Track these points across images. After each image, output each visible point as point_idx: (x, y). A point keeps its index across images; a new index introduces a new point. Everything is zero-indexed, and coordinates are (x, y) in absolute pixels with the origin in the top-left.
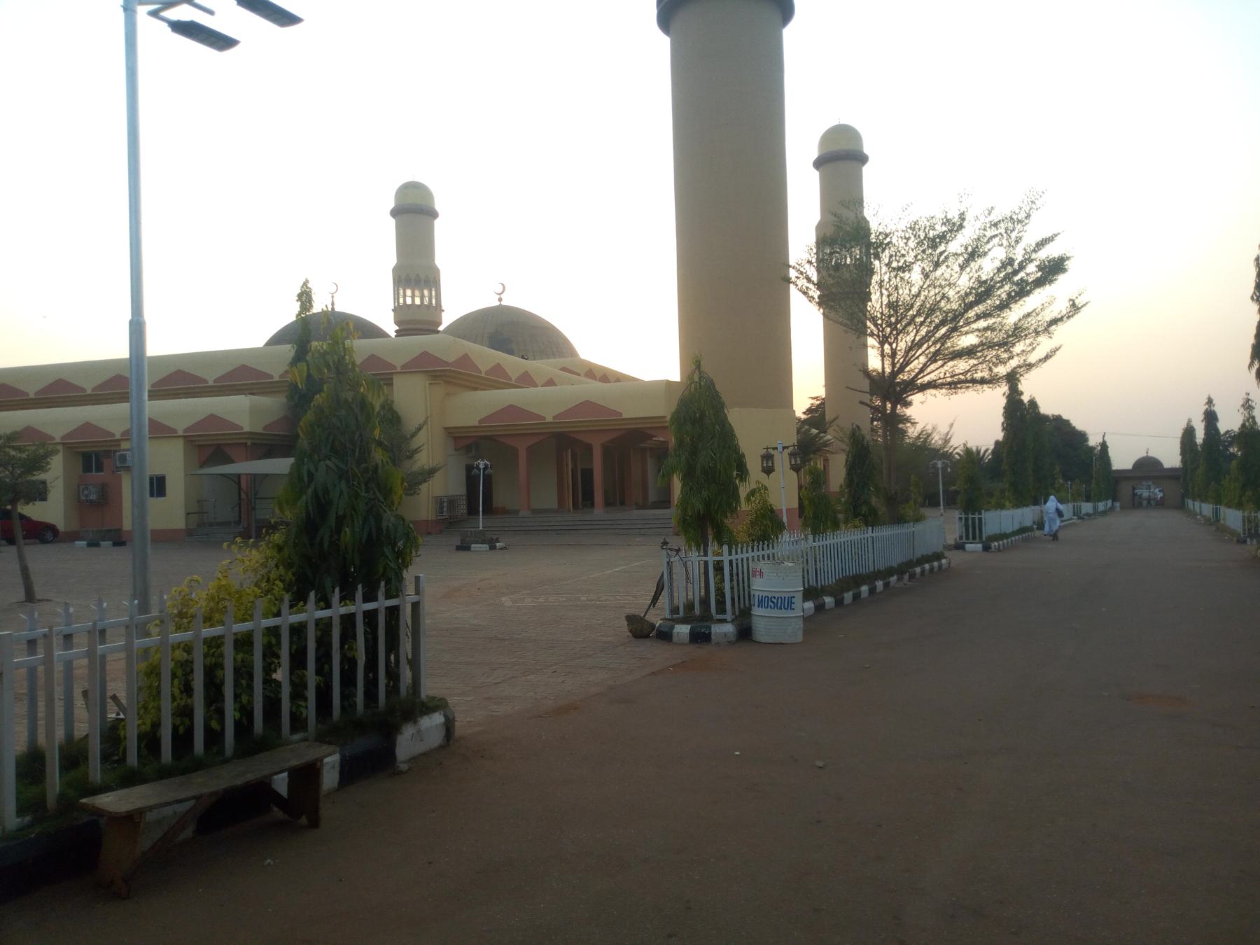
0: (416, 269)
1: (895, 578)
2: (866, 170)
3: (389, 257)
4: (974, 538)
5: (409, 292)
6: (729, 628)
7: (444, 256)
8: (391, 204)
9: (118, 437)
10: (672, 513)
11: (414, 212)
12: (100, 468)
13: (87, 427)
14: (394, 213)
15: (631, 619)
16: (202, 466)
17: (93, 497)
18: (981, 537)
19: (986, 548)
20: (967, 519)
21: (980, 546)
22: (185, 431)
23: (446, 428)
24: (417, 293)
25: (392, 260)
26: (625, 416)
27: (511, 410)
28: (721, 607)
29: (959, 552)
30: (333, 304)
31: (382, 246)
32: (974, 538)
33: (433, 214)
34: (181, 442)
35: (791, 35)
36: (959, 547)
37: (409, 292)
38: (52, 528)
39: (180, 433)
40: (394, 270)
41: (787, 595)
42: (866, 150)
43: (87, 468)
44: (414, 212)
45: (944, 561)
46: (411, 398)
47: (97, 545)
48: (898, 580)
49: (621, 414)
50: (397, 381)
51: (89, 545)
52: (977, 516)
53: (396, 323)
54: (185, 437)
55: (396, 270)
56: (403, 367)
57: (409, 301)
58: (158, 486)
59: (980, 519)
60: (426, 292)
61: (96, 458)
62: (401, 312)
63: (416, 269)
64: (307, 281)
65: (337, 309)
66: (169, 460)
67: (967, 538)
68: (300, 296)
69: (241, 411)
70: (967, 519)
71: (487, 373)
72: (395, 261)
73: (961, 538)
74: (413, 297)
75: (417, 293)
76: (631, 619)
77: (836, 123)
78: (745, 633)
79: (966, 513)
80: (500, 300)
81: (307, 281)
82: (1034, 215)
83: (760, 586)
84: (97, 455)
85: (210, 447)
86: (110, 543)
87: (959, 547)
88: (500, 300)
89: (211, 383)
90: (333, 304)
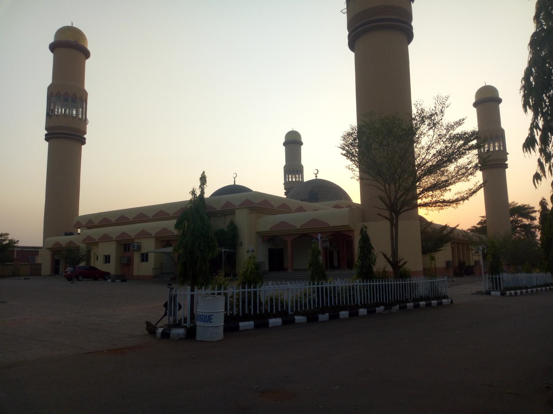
0: (293, 166)
1: (382, 308)
2: (501, 106)
3: (283, 162)
4: (497, 288)
5: (290, 176)
6: (181, 331)
7: (305, 160)
9: (133, 237)
11: (293, 143)
12: (129, 251)
13: (123, 234)
14: (285, 144)
15: (148, 324)
18: (500, 288)
19: (503, 294)
23: (257, 232)
24: (293, 176)
25: (284, 163)
26: (331, 225)
27: (283, 223)
28: (185, 322)
30: (235, 182)
32: (497, 288)
33: (301, 144)
34: (153, 240)
35: (412, 48)
36: (488, 293)
37: (290, 176)
38: (108, 274)
39: (153, 236)
40: (284, 167)
41: (208, 314)
42: (500, 96)
43: (125, 251)
44: (293, 143)
45: (444, 301)
46: (242, 219)
47: (114, 281)
48: (385, 309)
50: (237, 212)
52: (497, 276)
53: (285, 189)
54: (155, 237)
56: (239, 206)
57: (290, 180)
58: (145, 258)
59: (499, 278)
60: (297, 176)
61: (126, 246)
62: (288, 186)
63: (293, 166)
64: (204, 172)
65: (236, 184)
66: (148, 246)
67: (493, 288)
69: (170, 224)
70: (492, 278)
71: (277, 207)
72: (285, 164)
73: (490, 288)
74: (292, 178)
75: (293, 176)
76: (148, 324)
77: (483, 85)
78: (191, 333)
79: (492, 275)
80: (316, 176)
81: (204, 172)
82: (446, 111)
83: (200, 309)
85: (164, 240)
86: (120, 280)
88: (316, 176)
89: (171, 215)
90: (235, 182)
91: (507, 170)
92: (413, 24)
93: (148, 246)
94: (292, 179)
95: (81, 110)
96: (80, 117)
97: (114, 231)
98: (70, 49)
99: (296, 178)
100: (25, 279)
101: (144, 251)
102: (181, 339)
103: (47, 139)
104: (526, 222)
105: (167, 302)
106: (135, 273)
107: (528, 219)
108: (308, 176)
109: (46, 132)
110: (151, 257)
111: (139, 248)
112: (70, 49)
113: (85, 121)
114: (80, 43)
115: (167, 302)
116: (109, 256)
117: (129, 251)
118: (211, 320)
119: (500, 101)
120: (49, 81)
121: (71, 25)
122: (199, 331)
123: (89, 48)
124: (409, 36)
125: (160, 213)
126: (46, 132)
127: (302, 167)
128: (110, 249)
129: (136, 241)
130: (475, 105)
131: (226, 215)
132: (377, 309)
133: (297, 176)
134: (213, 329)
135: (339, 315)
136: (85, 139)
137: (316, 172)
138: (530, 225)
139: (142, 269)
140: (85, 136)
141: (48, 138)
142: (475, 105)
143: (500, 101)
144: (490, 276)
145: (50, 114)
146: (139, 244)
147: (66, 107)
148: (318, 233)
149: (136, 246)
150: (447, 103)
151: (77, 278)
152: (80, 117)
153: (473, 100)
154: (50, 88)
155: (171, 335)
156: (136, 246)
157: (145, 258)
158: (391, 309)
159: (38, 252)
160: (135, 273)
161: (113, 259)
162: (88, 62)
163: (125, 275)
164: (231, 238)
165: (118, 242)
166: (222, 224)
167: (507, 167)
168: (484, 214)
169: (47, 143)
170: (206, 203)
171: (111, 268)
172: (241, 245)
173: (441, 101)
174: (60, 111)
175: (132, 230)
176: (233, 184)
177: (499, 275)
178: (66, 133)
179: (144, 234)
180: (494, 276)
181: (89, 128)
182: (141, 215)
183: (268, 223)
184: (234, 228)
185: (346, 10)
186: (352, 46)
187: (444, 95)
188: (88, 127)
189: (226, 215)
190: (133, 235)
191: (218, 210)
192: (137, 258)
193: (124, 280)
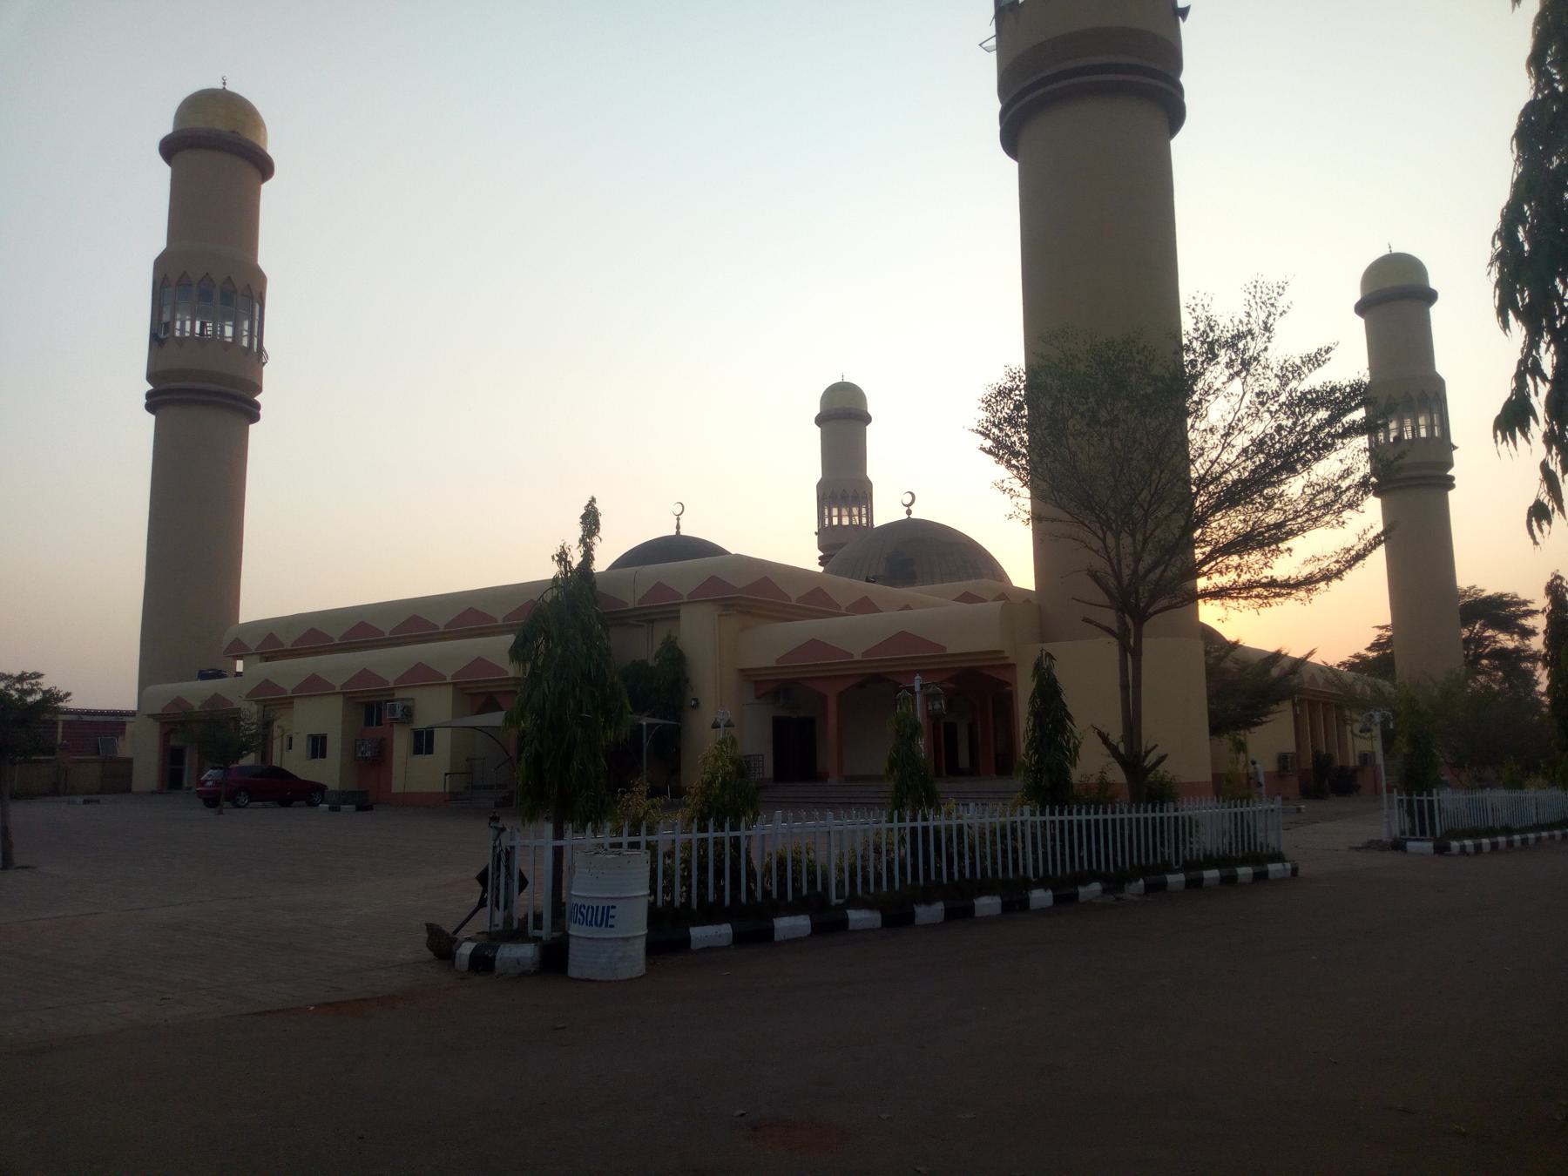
0: (844, 481)
1: (1096, 887)
2: (1435, 311)
3: (812, 470)
4: (1423, 832)
5: (835, 511)
6: (526, 952)
8: (816, 410)
9: (391, 685)
10: (1018, 782)
11: (843, 416)
12: (379, 723)
13: (365, 675)
14: (820, 420)
15: (434, 931)
16: (478, 713)
17: (368, 754)
19: (1441, 849)
20: (1410, 803)
21: (1431, 845)
22: (454, 677)
23: (742, 670)
24: (844, 512)
25: (817, 474)
26: (949, 651)
27: (814, 645)
29: (1391, 857)
30: (678, 527)
31: (804, 459)
32: (1423, 832)
33: (867, 419)
35: (1182, 148)
36: (1398, 846)
37: (835, 511)
38: (320, 789)
39: (449, 680)
41: (602, 904)
42: (1433, 284)
43: (368, 722)
44: (843, 416)
45: (1274, 868)
46: (699, 633)
47: (338, 809)
48: (1105, 891)
49: (944, 648)
50: (685, 613)
51: (331, 809)
52: (1425, 798)
53: (820, 548)
54: (454, 684)
55: (820, 486)
58: (423, 742)
59: (1431, 803)
60: (855, 511)
61: (373, 708)
62: (830, 539)
64: (593, 500)
65: (683, 533)
66: (435, 708)
67: (1413, 832)
68: (584, 517)
70: (1410, 803)
73: (1403, 833)
74: (840, 517)
75: (844, 512)
76: (434, 931)
77: (1384, 252)
78: (554, 958)
79: (1409, 794)
80: (909, 512)
81: (593, 500)
82: (1278, 325)
83: (580, 890)
84: (379, 705)
85: (477, 693)
87: (1398, 846)
88: (909, 512)
89: (500, 622)
90: (678, 527)
91: (252, 427)
92: (1185, 79)
93: (435, 708)
94: (840, 521)
95: (246, 325)
96: (245, 343)
97: (339, 667)
98: (217, 154)
99: (850, 516)
100: (85, 802)
101: (421, 723)
102: (524, 974)
103: (150, 407)
104: (1507, 641)
105: (486, 869)
106: (397, 786)
107: (1512, 634)
108: (886, 511)
109: (150, 387)
110: (442, 740)
111: (408, 714)
112: (217, 154)
113: (257, 356)
114: (248, 136)
115: (486, 869)
116: (324, 738)
117: (379, 723)
118: (611, 921)
119: (1431, 297)
120: (159, 243)
121: (220, 86)
122: (575, 950)
123: (272, 149)
124: (1174, 115)
125: (467, 614)
126: (150, 387)
127: (868, 485)
128: (327, 717)
129: (399, 695)
130: (1361, 309)
131: (652, 621)
132: (1081, 890)
133: (855, 511)
134: (615, 947)
135: (772, 929)
136: (258, 406)
137: (908, 499)
138: (1517, 650)
139: (415, 773)
140: (1450, 473)
141: (154, 403)
142: (1361, 309)
143: (1431, 297)
144: (1404, 797)
145: (160, 337)
146: (409, 703)
147: (205, 317)
148: (915, 672)
149: (399, 711)
150: (1281, 303)
151: (233, 799)
152: (245, 343)
153: (1356, 296)
154: (161, 264)
155: (497, 963)
156: (399, 711)
157: (423, 742)
158: (1122, 890)
159: (124, 724)
160: (397, 786)
161: (334, 747)
162: (266, 187)
163: (366, 793)
164: (667, 687)
165: (349, 697)
166: (641, 647)
167: (1452, 486)
168: (1387, 619)
169: (152, 418)
170: (599, 588)
171: (328, 772)
172: (696, 706)
173: (1265, 298)
174: (187, 326)
175: (389, 663)
176: (673, 533)
177: (1430, 794)
178: (204, 388)
179: (422, 676)
180: (1415, 797)
181: (269, 374)
182: (414, 622)
183: (771, 645)
184: (675, 658)
185: (993, 42)
186: (1011, 140)
187: (1272, 279)
188: (267, 371)
189: (652, 621)
190: (391, 677)
191: (631, 606)
192: (401, 742)
193: (364, 807)
